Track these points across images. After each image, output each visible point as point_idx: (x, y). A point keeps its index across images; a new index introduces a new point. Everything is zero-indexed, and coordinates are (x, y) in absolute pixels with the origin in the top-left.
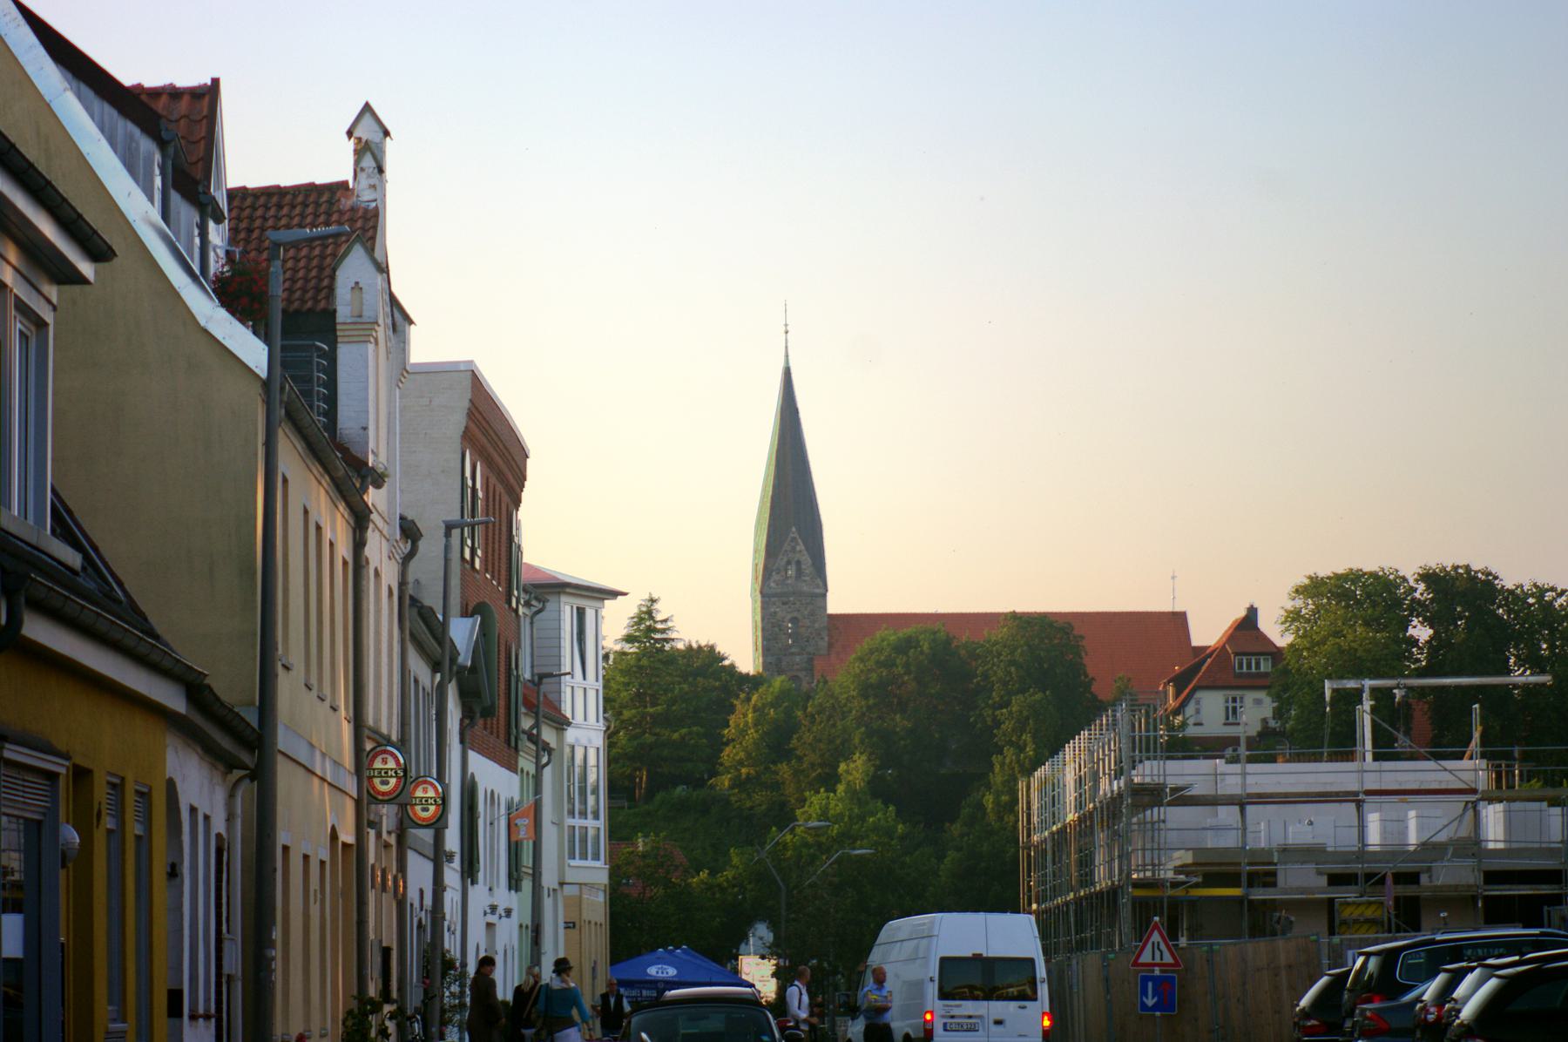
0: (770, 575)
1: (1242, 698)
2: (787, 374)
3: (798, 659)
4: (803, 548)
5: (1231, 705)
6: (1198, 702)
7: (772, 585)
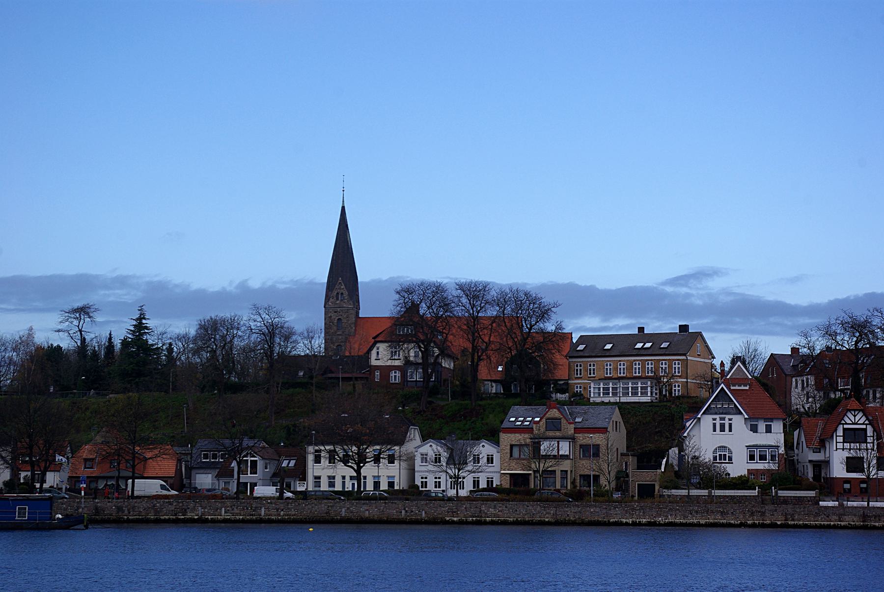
0: (329, 300)
2: (343, 208)
3: (340, 337)
4: (344, 287)
6: (378, 348)
7: (330, 304)
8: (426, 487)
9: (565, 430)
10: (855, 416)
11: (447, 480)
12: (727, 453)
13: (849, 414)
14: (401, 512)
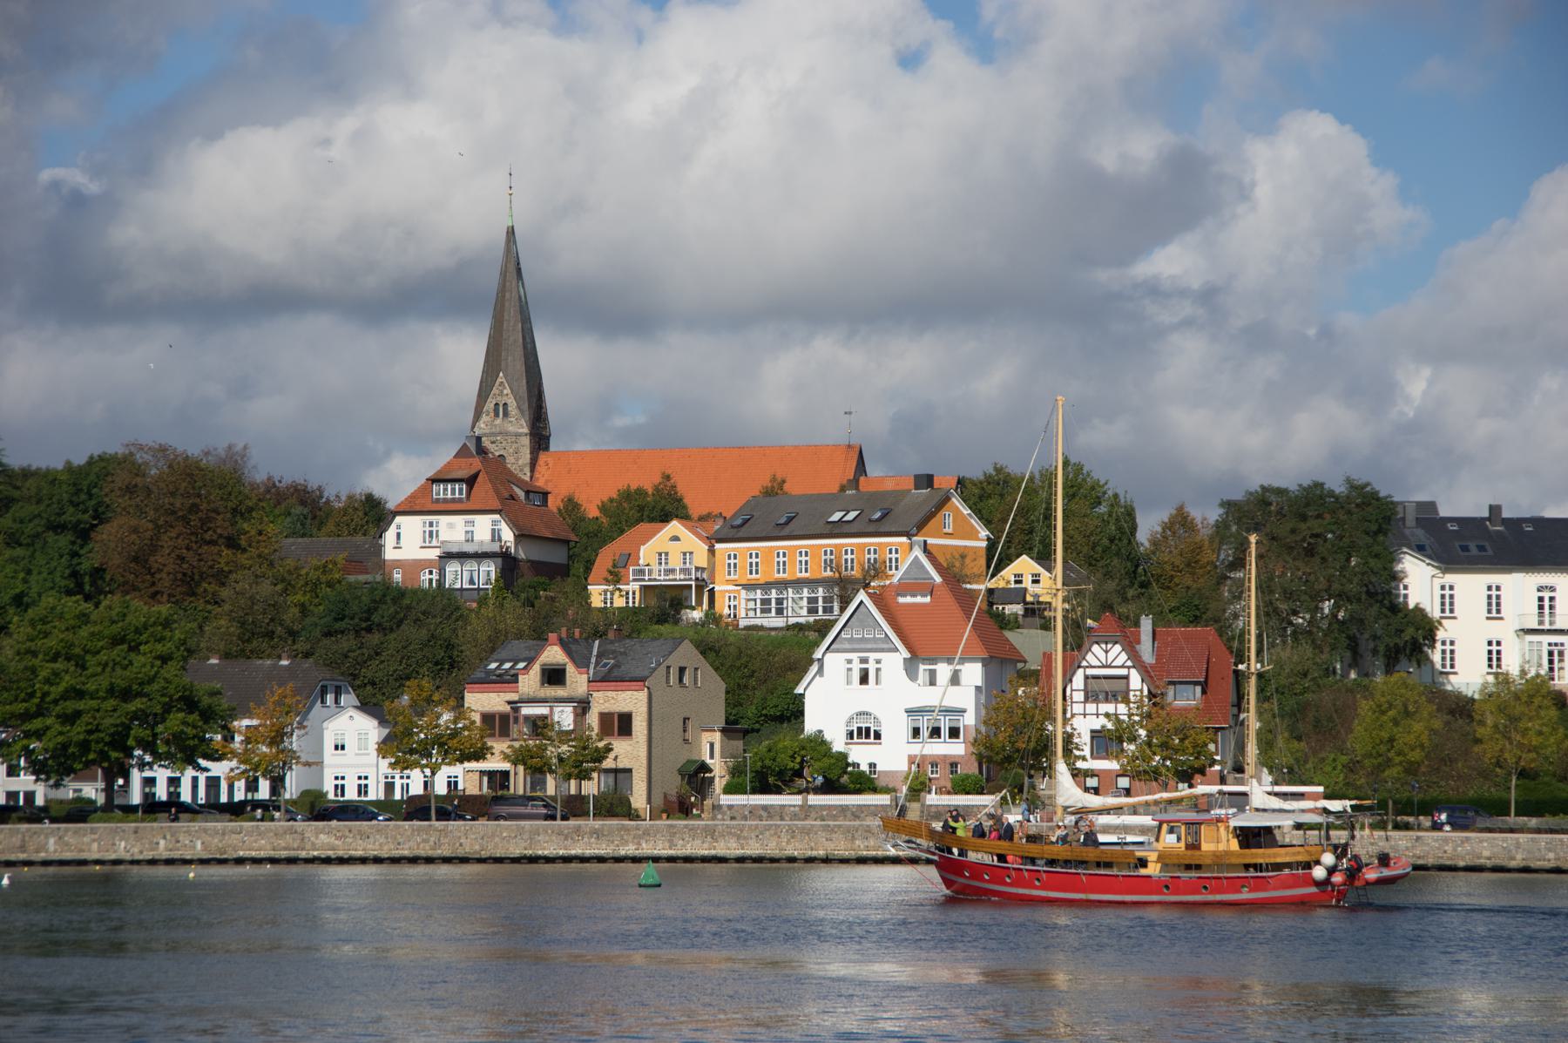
1: (437, 523)
5: (428, 529)
6: (399, 527)
7: (482, 426)
8: (343, 795)
9: (574, 685)
10: (1106, 652)
11: (378, 782)
12: (871, 726)
13: (1095, 648)
14: (158, 843)
